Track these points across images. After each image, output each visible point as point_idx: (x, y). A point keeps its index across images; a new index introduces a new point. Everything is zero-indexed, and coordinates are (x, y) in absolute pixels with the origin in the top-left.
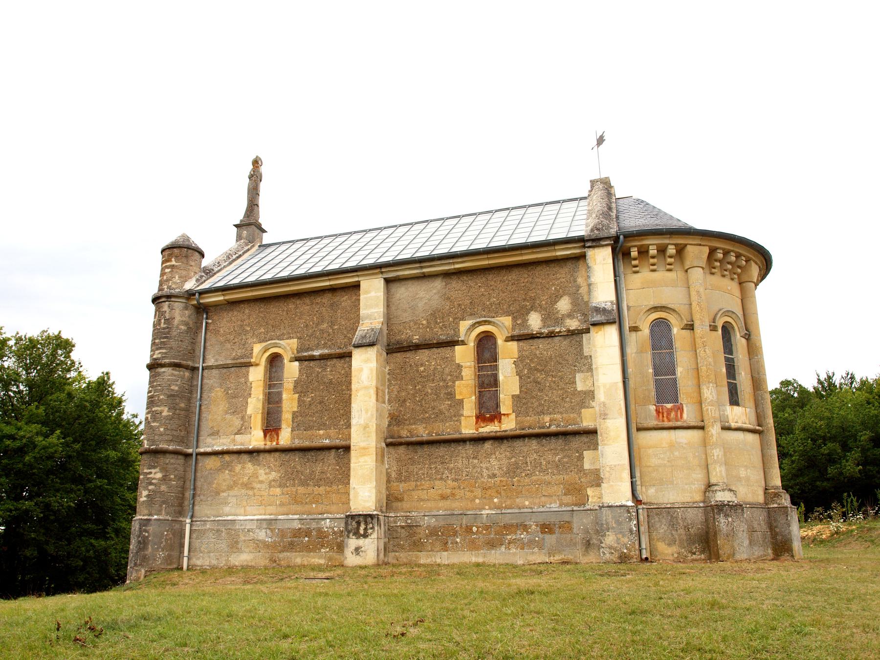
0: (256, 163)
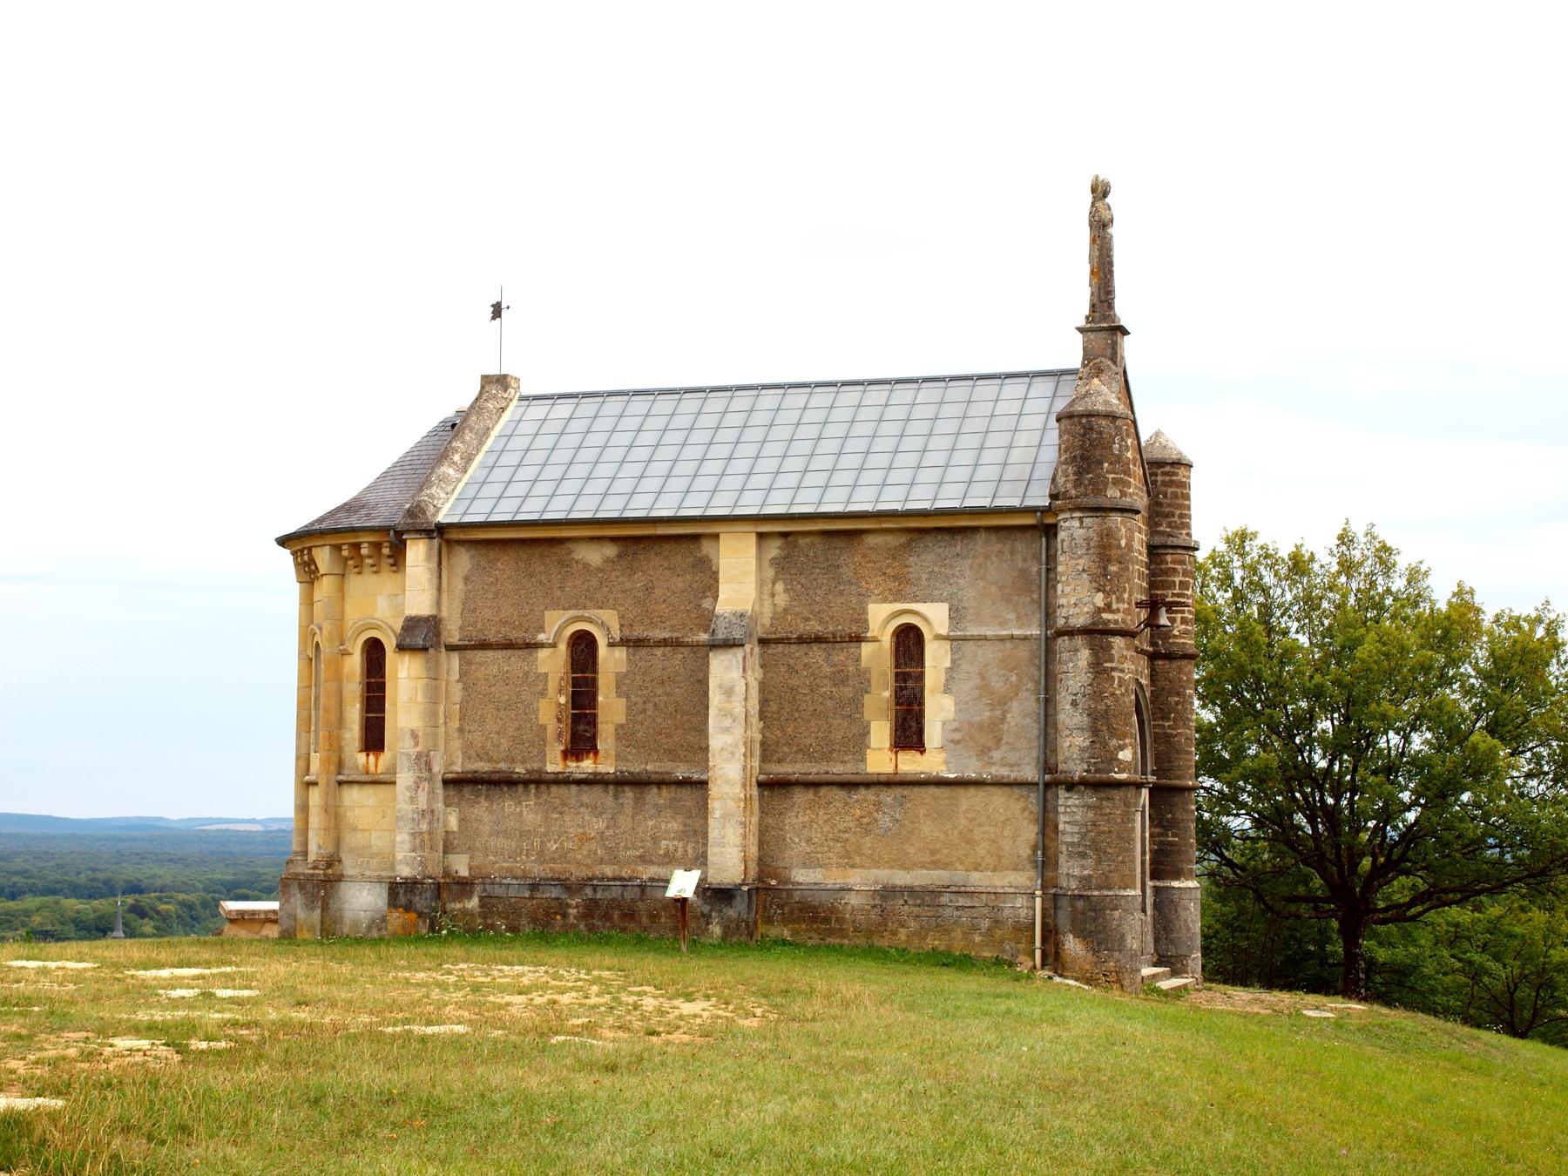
0: (1100, 191)
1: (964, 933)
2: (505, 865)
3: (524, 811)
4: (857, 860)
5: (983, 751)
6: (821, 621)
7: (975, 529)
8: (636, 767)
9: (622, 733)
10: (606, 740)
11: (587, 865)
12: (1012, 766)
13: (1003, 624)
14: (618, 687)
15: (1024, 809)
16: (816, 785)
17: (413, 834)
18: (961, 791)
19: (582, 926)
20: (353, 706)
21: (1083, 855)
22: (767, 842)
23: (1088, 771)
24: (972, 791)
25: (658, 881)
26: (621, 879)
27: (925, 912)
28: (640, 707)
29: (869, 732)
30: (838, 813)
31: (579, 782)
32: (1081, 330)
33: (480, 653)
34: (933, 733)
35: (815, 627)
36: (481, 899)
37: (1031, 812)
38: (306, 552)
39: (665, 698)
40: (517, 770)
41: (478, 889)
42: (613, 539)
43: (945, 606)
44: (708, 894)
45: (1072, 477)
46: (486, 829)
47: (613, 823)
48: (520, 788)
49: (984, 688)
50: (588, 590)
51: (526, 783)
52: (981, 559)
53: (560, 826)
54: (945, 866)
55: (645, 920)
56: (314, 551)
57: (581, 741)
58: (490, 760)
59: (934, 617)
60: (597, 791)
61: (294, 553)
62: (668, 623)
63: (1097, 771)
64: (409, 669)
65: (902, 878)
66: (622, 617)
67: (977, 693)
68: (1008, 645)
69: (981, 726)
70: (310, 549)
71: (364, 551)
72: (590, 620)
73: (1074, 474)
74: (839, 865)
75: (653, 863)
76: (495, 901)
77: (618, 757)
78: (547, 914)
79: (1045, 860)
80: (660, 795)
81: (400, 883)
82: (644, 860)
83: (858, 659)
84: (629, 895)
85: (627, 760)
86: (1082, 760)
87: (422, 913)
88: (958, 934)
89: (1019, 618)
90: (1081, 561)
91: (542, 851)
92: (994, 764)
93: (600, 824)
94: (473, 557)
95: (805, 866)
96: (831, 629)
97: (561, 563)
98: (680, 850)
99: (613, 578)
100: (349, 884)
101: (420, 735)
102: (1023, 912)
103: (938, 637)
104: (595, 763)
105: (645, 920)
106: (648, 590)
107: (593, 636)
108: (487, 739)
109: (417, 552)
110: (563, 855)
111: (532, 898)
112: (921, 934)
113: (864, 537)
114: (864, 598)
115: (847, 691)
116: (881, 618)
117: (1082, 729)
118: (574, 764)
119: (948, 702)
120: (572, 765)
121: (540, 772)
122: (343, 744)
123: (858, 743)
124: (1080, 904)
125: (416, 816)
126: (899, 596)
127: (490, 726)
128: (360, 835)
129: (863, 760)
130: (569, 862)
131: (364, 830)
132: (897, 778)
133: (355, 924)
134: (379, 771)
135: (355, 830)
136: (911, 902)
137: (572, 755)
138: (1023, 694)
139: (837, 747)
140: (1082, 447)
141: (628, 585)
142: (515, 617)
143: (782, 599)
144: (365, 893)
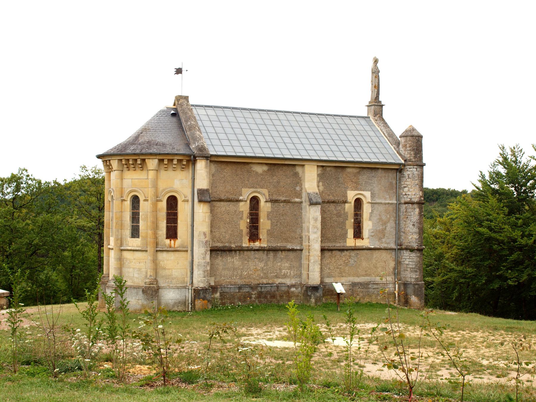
0: (376, 61)
1: (375, 296)
2: (228, 280)
3: (234, 261)
4: (344, 274)
5: (380, 239)
6: (333, 196)
7: (378, 168)
9: (270, 233)
10: (263, 234)
11: (257, 279)
12: (388, 243)
13: (385, 199)
14: (268, 217)
15: (391, 257)
16: (331, 250)
17: (204, 271)
18: (374, 251)
19: (257, 301)
20: (163, 221)
21: (416, 271)
22: (212, 272)
23: (418, 246)
24: (377, 251)
25: (282, 284)
26: (269, 284)
27: (364, 290)
28: (275, 223)
29: (347, 233)
30: (338, 259)
31: (255, 250)
32: (368, 106)
33: (218, 203)
35: (331, 198)
36: (220, 293)
37: (393, 258)
38: (108, 161)
39: (283, 221)
40: (232, 246)
41: (219, 290)
42: (266, 164)
43: (370, 192)
44: (310, 288)
45: (413, 155)
47: (266, 264)
48: (233, 252)
49: (380, 219)
50: (257, 182)
51: (235, 251)
52: (379, 178)
53: (248, 266)
54: (369, 275)
55: (278, 298)
56: (111, 161)
57: (254, 236)
58: (222, 242)
59: (366, 197)
60: (261, 252)
61: (103, 161)
62: (285, 195)
63: (420, 246)
64: (203, 209)
65: (357, 280)
66: (269, 192)
67: (378, 220)
68: (387, 206)
69: (379, 231)
70: (110, 160)
71: (131, 162)
72: (259, 193)
73: (414, 154)
74: (338, 276)
75: (279, 278)
76: (225, 294)
77: (268, 241)
78: (245, 297)
79: (397, 272)
80: (282, 254)
81: (201, 290)
82: (277, 277)
83: (344, 209)
84: (273, 290)
85: (271, 242)
86: (416, 242)
87: (210, 300)
88: (374, 297)
89: (390, 197)
90: (417, 182)
91: (241, 275)
92: (383, 243)
93: (261, 265)
94: (215, 167)
95: (328, 277)
96: (336, 198)
98: (289, 273)
99: (266, 178)
100: (164, 290)
101: (207, 234)
102: (391, 289)
103: (369, 203)
104: (260, 243)
105: (278, 298)
106: (278, 182)
108: (221, 235)
109: (201, 165)
110: (249, 276)
111: (239, 292)
112: (363, 297)
113: (347, 169)
114: (346, 189)
115: (341, 219)
116: (351, 195)
117: (416, 233)
118: (252, 244)
119: (370, 223)
120: (252, 244)
121: (240, 246)
122: (158, 236)
123: (344, 236)
124: (416, 286)
125: (205, 264)
126: (356, 189)
127: (223, 230)
129: (346, 242)
130: (250, 279)
131: (169, 269)
132: (356, 248)
133: (167, 305)
134: (176, 246)
135: (165, 269)
136: (361, 287)
137: (252, 240)
138: (391, 221)
139: (338, 238)
140: (416, 146)
141: (271, 181)
142: (231, 190)
143: (321, 188)
144: (171, 293)
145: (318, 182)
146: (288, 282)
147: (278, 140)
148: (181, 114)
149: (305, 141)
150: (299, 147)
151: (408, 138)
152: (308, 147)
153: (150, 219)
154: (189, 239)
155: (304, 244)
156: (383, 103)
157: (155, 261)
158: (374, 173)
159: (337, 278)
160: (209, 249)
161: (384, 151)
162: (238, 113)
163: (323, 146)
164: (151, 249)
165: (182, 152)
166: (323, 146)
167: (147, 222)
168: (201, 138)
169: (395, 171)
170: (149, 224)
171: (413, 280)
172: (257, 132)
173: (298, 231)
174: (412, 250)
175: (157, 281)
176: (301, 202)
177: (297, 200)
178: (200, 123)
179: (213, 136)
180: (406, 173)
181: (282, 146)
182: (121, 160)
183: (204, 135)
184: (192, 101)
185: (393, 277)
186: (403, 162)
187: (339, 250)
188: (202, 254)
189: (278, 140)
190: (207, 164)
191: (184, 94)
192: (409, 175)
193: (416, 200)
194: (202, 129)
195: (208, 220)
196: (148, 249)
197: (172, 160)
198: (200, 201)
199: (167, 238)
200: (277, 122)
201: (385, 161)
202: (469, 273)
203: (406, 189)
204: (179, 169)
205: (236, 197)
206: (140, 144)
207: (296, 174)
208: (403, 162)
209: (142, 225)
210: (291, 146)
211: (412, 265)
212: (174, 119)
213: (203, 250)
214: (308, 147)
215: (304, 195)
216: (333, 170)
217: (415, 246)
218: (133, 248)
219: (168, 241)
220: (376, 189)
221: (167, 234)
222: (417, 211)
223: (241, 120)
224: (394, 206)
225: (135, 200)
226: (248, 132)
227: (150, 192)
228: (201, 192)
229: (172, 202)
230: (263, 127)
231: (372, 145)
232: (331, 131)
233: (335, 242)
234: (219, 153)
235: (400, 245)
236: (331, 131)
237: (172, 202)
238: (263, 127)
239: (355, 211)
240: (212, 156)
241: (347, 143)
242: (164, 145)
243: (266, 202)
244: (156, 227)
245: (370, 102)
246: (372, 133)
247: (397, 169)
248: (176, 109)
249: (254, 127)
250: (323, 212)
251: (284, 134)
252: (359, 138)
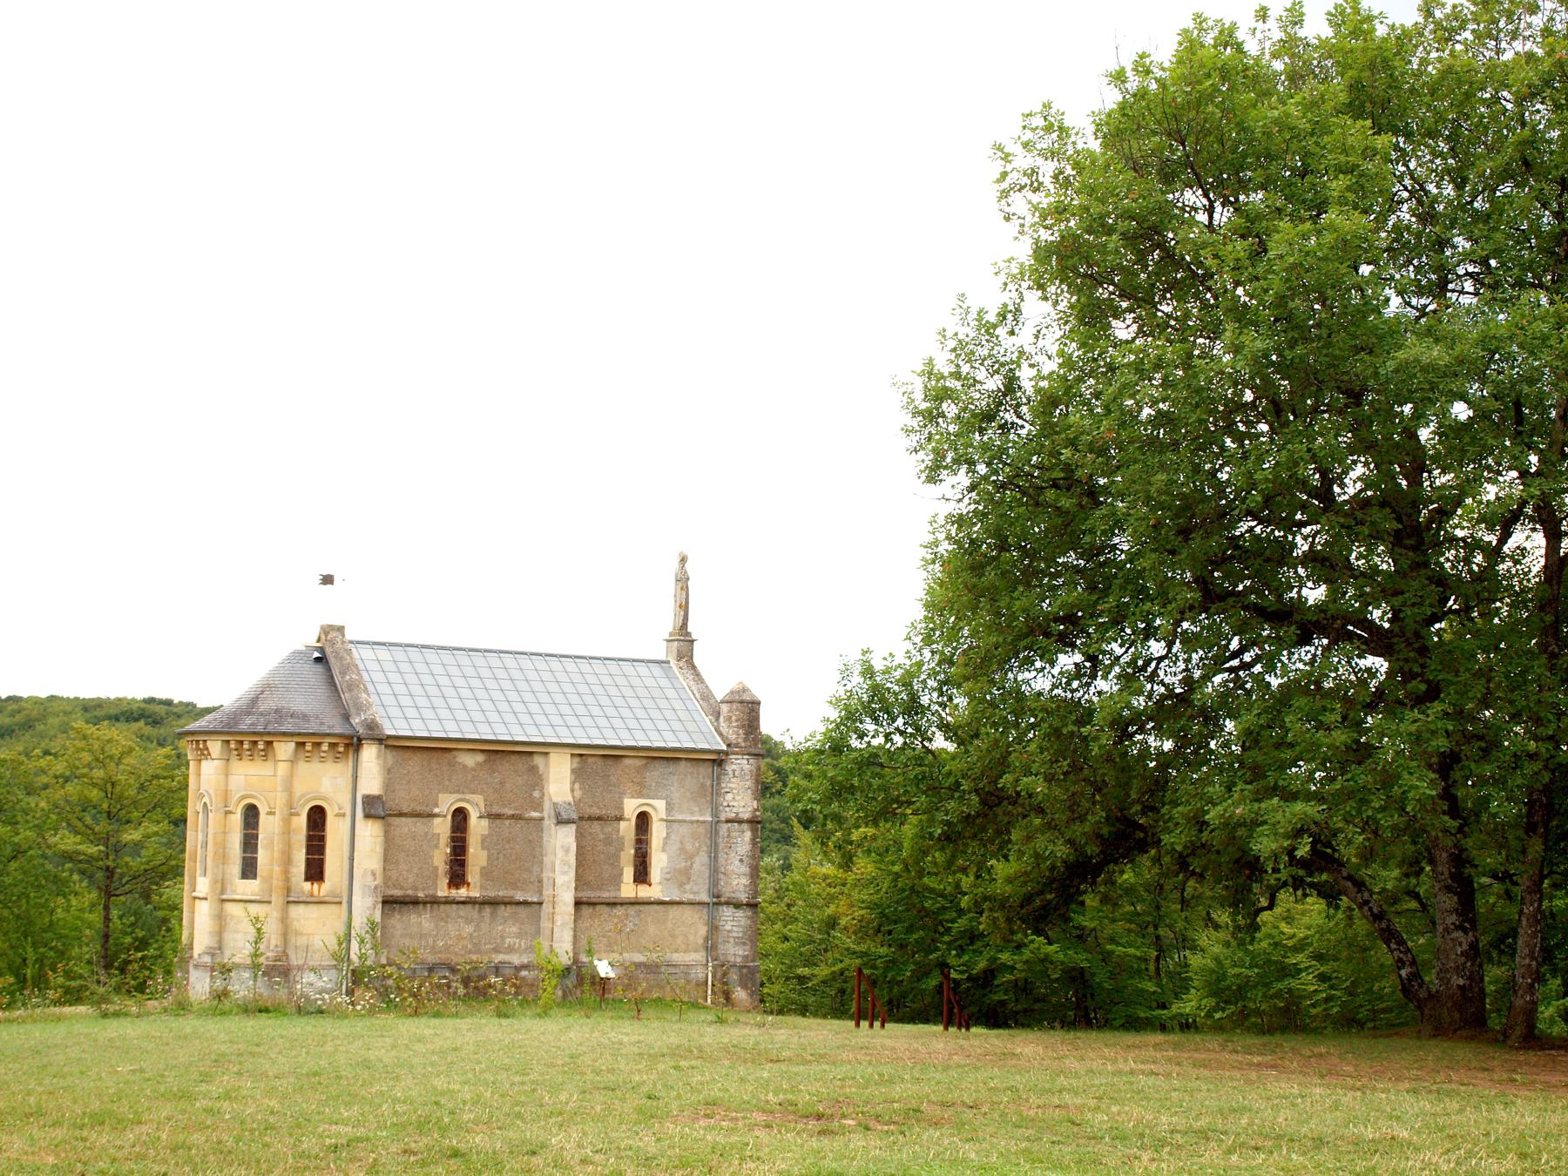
0: (683, 560)
3: (422, 921)
5: (681, 885)
6: (599, 807)
7: (679, 759)
8: (492, 894)
9: (486, 873)
10: (473, 875)
13: (692, 814)
18: (669, 907)
21: (745, 944)
24: (675, 907)
27: (651, 976)
31: (458, 903)
32: (668, 641)
33: (397, 819)
34: (656, 873)
35: (595, 811)
42: (482, 751)
46: (398, 933)
49: (682, 850)
51: (425, 903)
57: (457, 877)
58: (402, 888)
59: (658, 808)
60: (469, 907)
69: (680, 871)
71: (246, 746)
72: (468, 801)
77: (481, 887)
79: (711, 946)
82: (497, 951)
93: (469, 929)
97: (450, 764)
102: (700, 975)
106: (502, 783)
107: (312, 809)
109: (369, 753)
110: (447, 948)
112: (649, 990)
114: (622, 795)
116: (631, 807)
119: (664, 857)
121: (434, 896)
123: (617, 880)
124: (745, 971)
126: (640, 795)
127: (403, 867)
128: (305, 938)
138: (702, 853)
143: (578, 794)
145: (573, 783)
146: (516, 960)
147: (503, 707)
148: (332, 660)
149: (550, 709)
150: (541, 719)
151: (735, 706)
152: (556, 720)
153: (278, 846)
154: (346, 883)
155: (545, 892)
156: (694, 637)
157: (284, 921)
158: (672, 767)
159: (603, 955)
160: (380, 899)
161: (691, 727)
162: (431, 656)
163: (582, 719)
164: (277, 899)
165: (338, 730)
166: (582, 719)
167: (273, 851)
168: (369, 705)
169: (710, 763)
170: (276, 855)
171: (739, 960)
172: (465, 693)
173: (536, 869)
174: (738, 906)
175: (287, 956)
176: (542, 819)
177: (535, 814)
178: (365, 676)
179: (389, 700)
180: (729, 768)
181: (510, 718)
182: (228, 742)
183: (374, 699)
184: (349, 636)
185: (704, 954)
186: (725, 748)
187: (608, 904)
188: (368, 908)
189: (503, 707)
190: (379, 751)
191: (337, 622)
192: (734, 771)
193: (746, 816)
194: (370, 688)
195: (379, 849)
196: (273, 899)
197: (319, 744)
198: (367, 816)
199: (307, 879)
200: (501, 674)
201: (692, 745)
202: (880, 957)
203: (729, 796)
204: (330, 758)
205: (428, 809)
206: (261, 714)
207: (533, 770)
208: (725, 748)
209: (262, 856)
210: (525, 719)
211: (737, 932)
212: (319, 668)
213: (369, 901)
214: (556, 720)
215: (547, 806)
216: (600, 762)
217: (743, 898)
218: (245, 897)
219: (307, 885)
220: (676, 796)
221: (306, 873)
222: (748, 835)
223: (438, 669)
224: (708, 827)
225: (251, 813)
226: (450, 692)
227: (280, 799)
228: (369, 801)
229: (317, 817)
230: (475, 683)
231: (669, 715)
232: (598, 690)
233: (601, 889)
234: (402, 733)
235: (718, 897)
236: (598, 690)
237: (317, 817)
238: (475, 683)
239: (637, 835)
240: (389, 737)
241: (626, 713)
242: (305, 717)
243: (480, 817)
244: (287, 861)
245: (671, 634)
246: (671, 693)
247: (714, 760)
248: (321, 650)
249: (459, 682)
250: (580, 836)
251: (513, 696)
252: (649, 703)
